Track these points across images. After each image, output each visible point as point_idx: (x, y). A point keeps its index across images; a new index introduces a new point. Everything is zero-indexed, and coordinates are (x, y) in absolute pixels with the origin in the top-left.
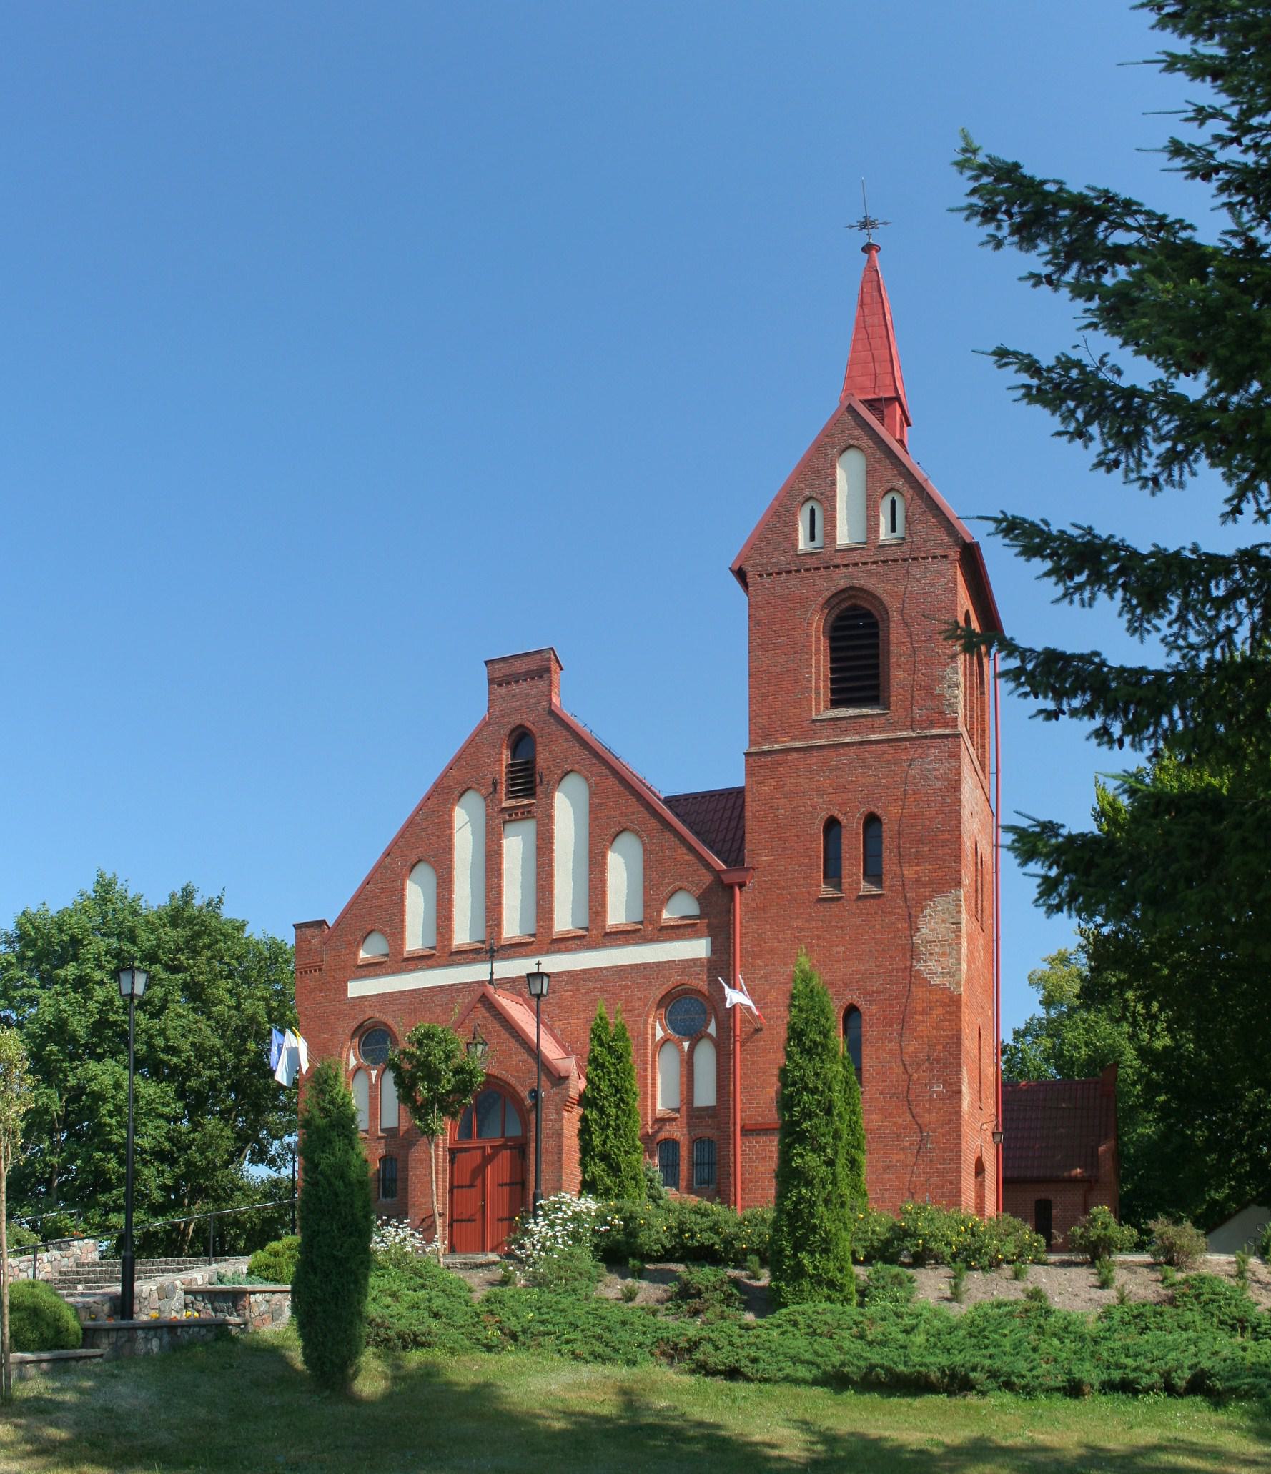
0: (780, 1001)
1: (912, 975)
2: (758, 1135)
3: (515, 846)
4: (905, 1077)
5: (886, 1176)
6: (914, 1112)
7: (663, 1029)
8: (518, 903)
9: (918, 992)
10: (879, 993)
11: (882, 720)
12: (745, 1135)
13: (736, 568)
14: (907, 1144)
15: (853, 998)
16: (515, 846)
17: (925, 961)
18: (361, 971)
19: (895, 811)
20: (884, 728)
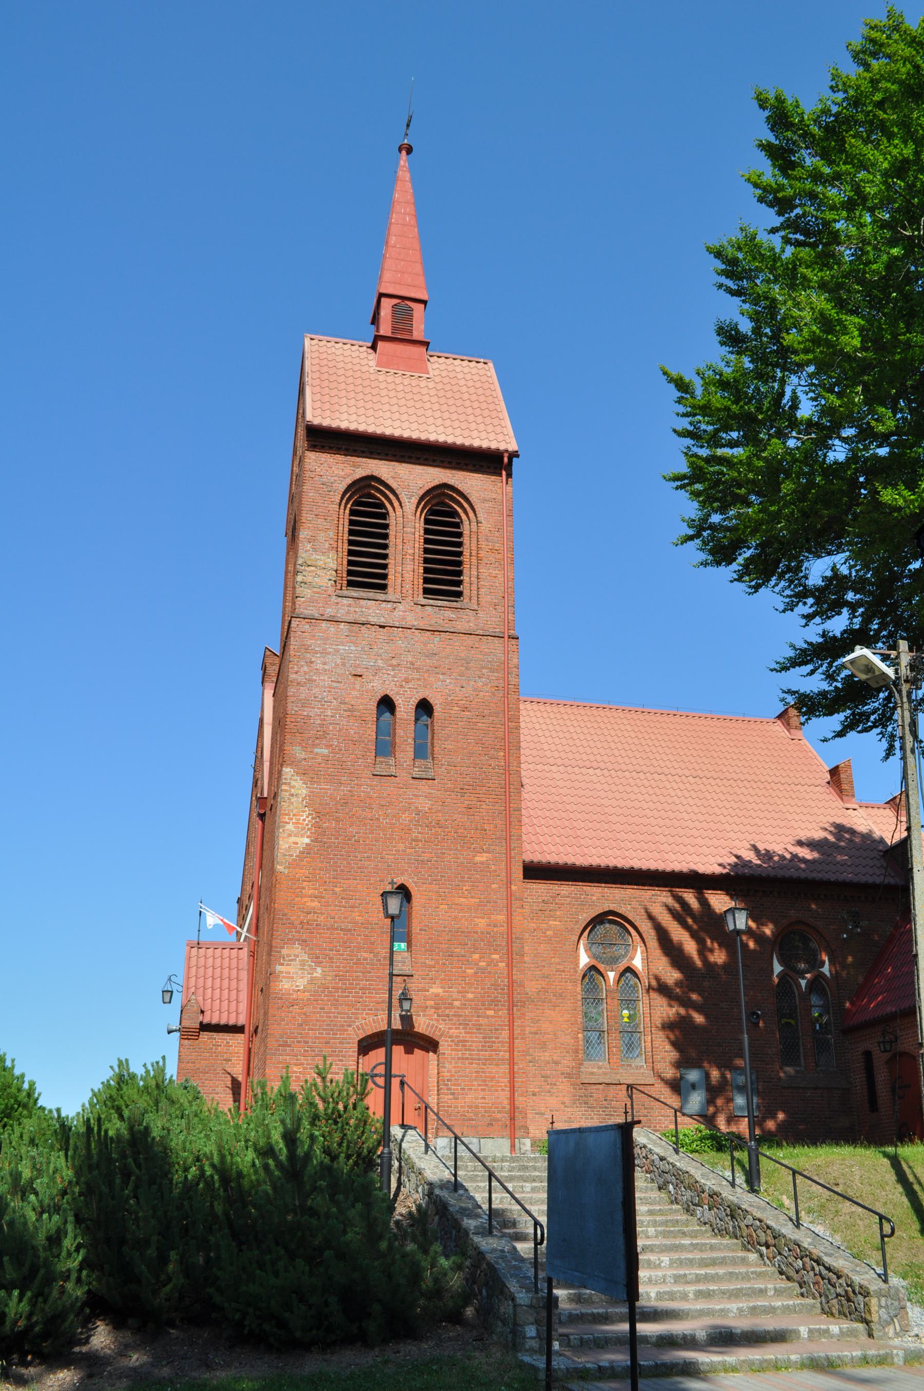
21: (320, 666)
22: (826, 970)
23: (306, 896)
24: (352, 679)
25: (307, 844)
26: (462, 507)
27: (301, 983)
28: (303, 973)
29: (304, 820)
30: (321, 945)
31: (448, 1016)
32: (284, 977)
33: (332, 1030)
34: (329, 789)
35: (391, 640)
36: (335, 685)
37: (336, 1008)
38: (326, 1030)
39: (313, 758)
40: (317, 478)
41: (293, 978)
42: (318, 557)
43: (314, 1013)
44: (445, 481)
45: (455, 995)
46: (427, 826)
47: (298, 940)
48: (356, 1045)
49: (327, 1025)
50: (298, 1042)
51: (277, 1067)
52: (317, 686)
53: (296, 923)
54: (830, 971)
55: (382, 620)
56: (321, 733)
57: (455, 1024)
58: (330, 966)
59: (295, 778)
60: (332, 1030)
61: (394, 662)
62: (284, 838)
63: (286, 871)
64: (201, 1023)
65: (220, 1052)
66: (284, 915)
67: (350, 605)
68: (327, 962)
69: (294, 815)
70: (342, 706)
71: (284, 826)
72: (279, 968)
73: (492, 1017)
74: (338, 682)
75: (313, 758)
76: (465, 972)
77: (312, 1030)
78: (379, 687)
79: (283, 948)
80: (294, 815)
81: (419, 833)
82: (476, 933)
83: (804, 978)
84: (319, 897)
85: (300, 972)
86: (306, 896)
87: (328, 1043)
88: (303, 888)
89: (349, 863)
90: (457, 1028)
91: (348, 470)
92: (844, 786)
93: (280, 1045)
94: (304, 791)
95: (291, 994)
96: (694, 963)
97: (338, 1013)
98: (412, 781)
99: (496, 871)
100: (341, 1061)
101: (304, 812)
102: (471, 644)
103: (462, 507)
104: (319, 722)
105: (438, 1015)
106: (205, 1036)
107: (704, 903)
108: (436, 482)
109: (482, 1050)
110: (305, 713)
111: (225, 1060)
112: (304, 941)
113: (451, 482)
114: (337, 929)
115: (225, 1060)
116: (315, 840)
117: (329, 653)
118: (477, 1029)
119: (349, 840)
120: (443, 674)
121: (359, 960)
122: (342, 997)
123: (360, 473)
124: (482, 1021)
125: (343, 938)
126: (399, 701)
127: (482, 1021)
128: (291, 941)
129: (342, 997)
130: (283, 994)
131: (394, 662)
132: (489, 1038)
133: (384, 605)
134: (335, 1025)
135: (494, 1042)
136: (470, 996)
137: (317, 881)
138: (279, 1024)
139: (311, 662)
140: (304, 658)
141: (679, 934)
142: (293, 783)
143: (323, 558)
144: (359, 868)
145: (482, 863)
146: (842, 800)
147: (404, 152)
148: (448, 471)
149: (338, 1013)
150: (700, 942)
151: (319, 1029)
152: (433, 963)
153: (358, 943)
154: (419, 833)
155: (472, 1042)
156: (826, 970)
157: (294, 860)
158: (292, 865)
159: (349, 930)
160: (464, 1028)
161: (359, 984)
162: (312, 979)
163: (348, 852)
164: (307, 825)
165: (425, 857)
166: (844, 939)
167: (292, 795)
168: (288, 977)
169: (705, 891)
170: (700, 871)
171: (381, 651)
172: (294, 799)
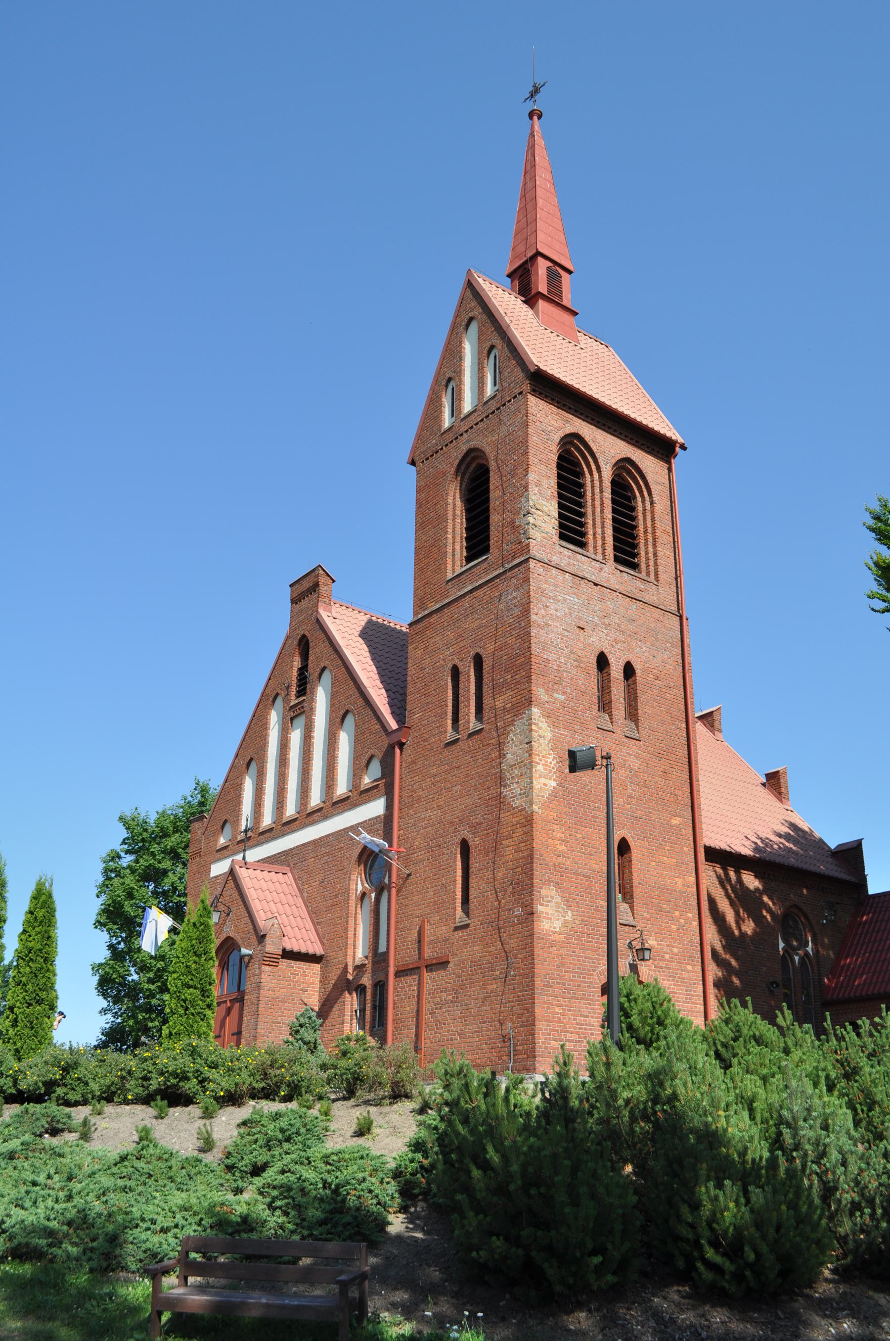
0: (451, 635)
1: (500, 799)
2: (407, 975)
3: (296, 737)
4: (496, 903)
5: (484, 1008)
6: (503, 939)
7: (362, 884)
8: (275, 752)
9: (505, 817)
10: (481, 823)
11: (485, 565)
12: (399, 977)
13: (410, 461)
14: (498, 973)
15: (465, 833)
16: (296, 737)
17: (509, 786)
18: (218, 855)
19: (491, 647)
20: (486, 571)
21: (553, 612)
22: (809, 949)
23: (556, 839)
24: (578, 631)
25: (554, 788)
26: (637, 483)
27: (557, 925)
28: (558, 915)
29: (551, 763)
30: (569, 889)
31: (661, 967)
32: (544, 918)
33: (582, 973)
34: (567, 736)
35: (602, 600)
36: (566, 633)
37: (584, 953)
38: (576, 973)
39: (554, 703)
40: (538, 424)
41: (550, 919)
42: (544, 503)
43: (568, 955)
44: (629, 455)
45: (666, 949)
46: (637, 784)
47: (553, 882)
48: (600, 990)
49: (579, 968)
50: (558, 983)
51: (543, 1007)
52: (553, 632)
53: (551, 864)
54: (812, 950)
55: (594, 577)
56: (558, 679)
57: (666, 976)
58: (578, 911)
59: (542, 719)
60: (582, 973)
61: (606, 621)
62: (536, 778)
63: (540, 811)
64: (284, 950)
65: (297, 982)
66: (541, 855)
67: (569, 557)
68: (575, 906)
69: (543, 757)
70: (572, 655)
71: (536, 767)
72: (540, 908)
73: (691, 971)
74: (568, 631)
75: (554, 703)
76: (670, 927)
77: (568, 972)
78: (599, 641)
79: (542, 888)
80: (543, 757)
81: (632, 790)
82: (676, 891)
83: (797, 954)
84: (565, 841)
85: (556, 914)
86: (556, 839)
87: (579, 986)
88: (554, 831)
89: (585, 811)
90: (668, 980)
91: (560, 423)
92: (783, 790)
93: (544, 986)
94: (549, 734)
95: (550, 935)
96: (733, 932)
97: (586, 957)
98: (625, 740)
99: (685, 835)
100: (590, 1004)
101: (550, 754)
102: (657, 616)
103: (637, 483)
104: (555, 667)
105: (656, 967)
106: (284, 963)
107: (740, 880)
108: (623, 455)
109: (685, 1002)
110: (545, 657)
111: (302, 990)
112: (557, 883)
113: (634, 458)
114: (580, 875)
115: (302, 990)
116: (559, 785)
117: (559, 601)
118: (682, 982)
119: (585, 788)
120: (641, 641)
121: (597, 906)
122: (587, 941)
123: (569, 429)
124: (685, 975)
125: (584, 884)
126: (612, 659)
127: (685, 975)
128: (547, 882)
129: (587, 941)
130: (544, 934)
131: (606, 621)
132: (690, 991)
133: (594, 563)
134: (584, 969)
135: (693, 995)
136: (675, 950)
137: (563, 825)
138: (543, 964)
139: (547, 607)
140: (541, 601)
141: (724, 905)
142: (540, 724)
143: (547, 504)
144: (593, 817)
145: (676, 826)
146: (781, 802)
147: (535, 118)
148: (630, 446)
149: (586, 957)
150: (737, 914)
151: (572, 972)
152: (648, 916)
153: (596, 890)
154: (632, 790)
155: (679, 993)
156: (809, 949)
157: (545, 802)
158: (544, 806)
159: (589, 877)
160: (673, 980)
161: (598, 931)
162: (565, 922)
163: (584, 800)
164: (553, 768)
165: (638, 814)
166: (823, 924)
167: (540, 736)
168: (548, 918)
169: (729, 868)
170: (742, 853)
171: (596, 608)
172: (542, 741)
